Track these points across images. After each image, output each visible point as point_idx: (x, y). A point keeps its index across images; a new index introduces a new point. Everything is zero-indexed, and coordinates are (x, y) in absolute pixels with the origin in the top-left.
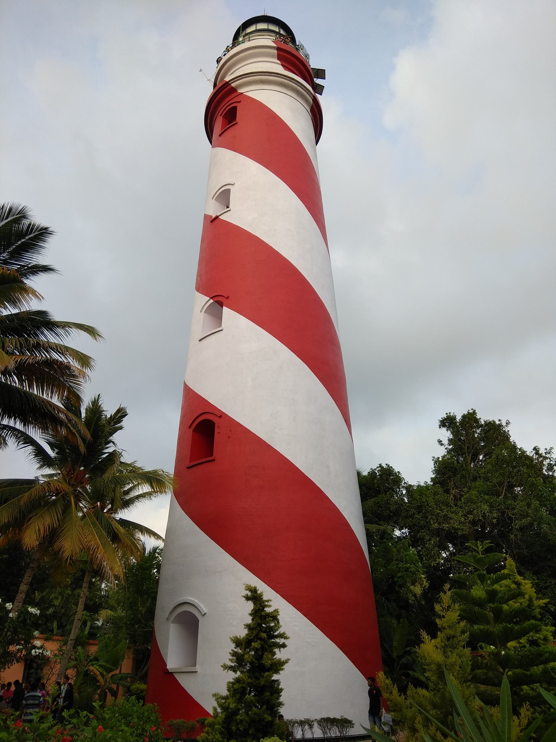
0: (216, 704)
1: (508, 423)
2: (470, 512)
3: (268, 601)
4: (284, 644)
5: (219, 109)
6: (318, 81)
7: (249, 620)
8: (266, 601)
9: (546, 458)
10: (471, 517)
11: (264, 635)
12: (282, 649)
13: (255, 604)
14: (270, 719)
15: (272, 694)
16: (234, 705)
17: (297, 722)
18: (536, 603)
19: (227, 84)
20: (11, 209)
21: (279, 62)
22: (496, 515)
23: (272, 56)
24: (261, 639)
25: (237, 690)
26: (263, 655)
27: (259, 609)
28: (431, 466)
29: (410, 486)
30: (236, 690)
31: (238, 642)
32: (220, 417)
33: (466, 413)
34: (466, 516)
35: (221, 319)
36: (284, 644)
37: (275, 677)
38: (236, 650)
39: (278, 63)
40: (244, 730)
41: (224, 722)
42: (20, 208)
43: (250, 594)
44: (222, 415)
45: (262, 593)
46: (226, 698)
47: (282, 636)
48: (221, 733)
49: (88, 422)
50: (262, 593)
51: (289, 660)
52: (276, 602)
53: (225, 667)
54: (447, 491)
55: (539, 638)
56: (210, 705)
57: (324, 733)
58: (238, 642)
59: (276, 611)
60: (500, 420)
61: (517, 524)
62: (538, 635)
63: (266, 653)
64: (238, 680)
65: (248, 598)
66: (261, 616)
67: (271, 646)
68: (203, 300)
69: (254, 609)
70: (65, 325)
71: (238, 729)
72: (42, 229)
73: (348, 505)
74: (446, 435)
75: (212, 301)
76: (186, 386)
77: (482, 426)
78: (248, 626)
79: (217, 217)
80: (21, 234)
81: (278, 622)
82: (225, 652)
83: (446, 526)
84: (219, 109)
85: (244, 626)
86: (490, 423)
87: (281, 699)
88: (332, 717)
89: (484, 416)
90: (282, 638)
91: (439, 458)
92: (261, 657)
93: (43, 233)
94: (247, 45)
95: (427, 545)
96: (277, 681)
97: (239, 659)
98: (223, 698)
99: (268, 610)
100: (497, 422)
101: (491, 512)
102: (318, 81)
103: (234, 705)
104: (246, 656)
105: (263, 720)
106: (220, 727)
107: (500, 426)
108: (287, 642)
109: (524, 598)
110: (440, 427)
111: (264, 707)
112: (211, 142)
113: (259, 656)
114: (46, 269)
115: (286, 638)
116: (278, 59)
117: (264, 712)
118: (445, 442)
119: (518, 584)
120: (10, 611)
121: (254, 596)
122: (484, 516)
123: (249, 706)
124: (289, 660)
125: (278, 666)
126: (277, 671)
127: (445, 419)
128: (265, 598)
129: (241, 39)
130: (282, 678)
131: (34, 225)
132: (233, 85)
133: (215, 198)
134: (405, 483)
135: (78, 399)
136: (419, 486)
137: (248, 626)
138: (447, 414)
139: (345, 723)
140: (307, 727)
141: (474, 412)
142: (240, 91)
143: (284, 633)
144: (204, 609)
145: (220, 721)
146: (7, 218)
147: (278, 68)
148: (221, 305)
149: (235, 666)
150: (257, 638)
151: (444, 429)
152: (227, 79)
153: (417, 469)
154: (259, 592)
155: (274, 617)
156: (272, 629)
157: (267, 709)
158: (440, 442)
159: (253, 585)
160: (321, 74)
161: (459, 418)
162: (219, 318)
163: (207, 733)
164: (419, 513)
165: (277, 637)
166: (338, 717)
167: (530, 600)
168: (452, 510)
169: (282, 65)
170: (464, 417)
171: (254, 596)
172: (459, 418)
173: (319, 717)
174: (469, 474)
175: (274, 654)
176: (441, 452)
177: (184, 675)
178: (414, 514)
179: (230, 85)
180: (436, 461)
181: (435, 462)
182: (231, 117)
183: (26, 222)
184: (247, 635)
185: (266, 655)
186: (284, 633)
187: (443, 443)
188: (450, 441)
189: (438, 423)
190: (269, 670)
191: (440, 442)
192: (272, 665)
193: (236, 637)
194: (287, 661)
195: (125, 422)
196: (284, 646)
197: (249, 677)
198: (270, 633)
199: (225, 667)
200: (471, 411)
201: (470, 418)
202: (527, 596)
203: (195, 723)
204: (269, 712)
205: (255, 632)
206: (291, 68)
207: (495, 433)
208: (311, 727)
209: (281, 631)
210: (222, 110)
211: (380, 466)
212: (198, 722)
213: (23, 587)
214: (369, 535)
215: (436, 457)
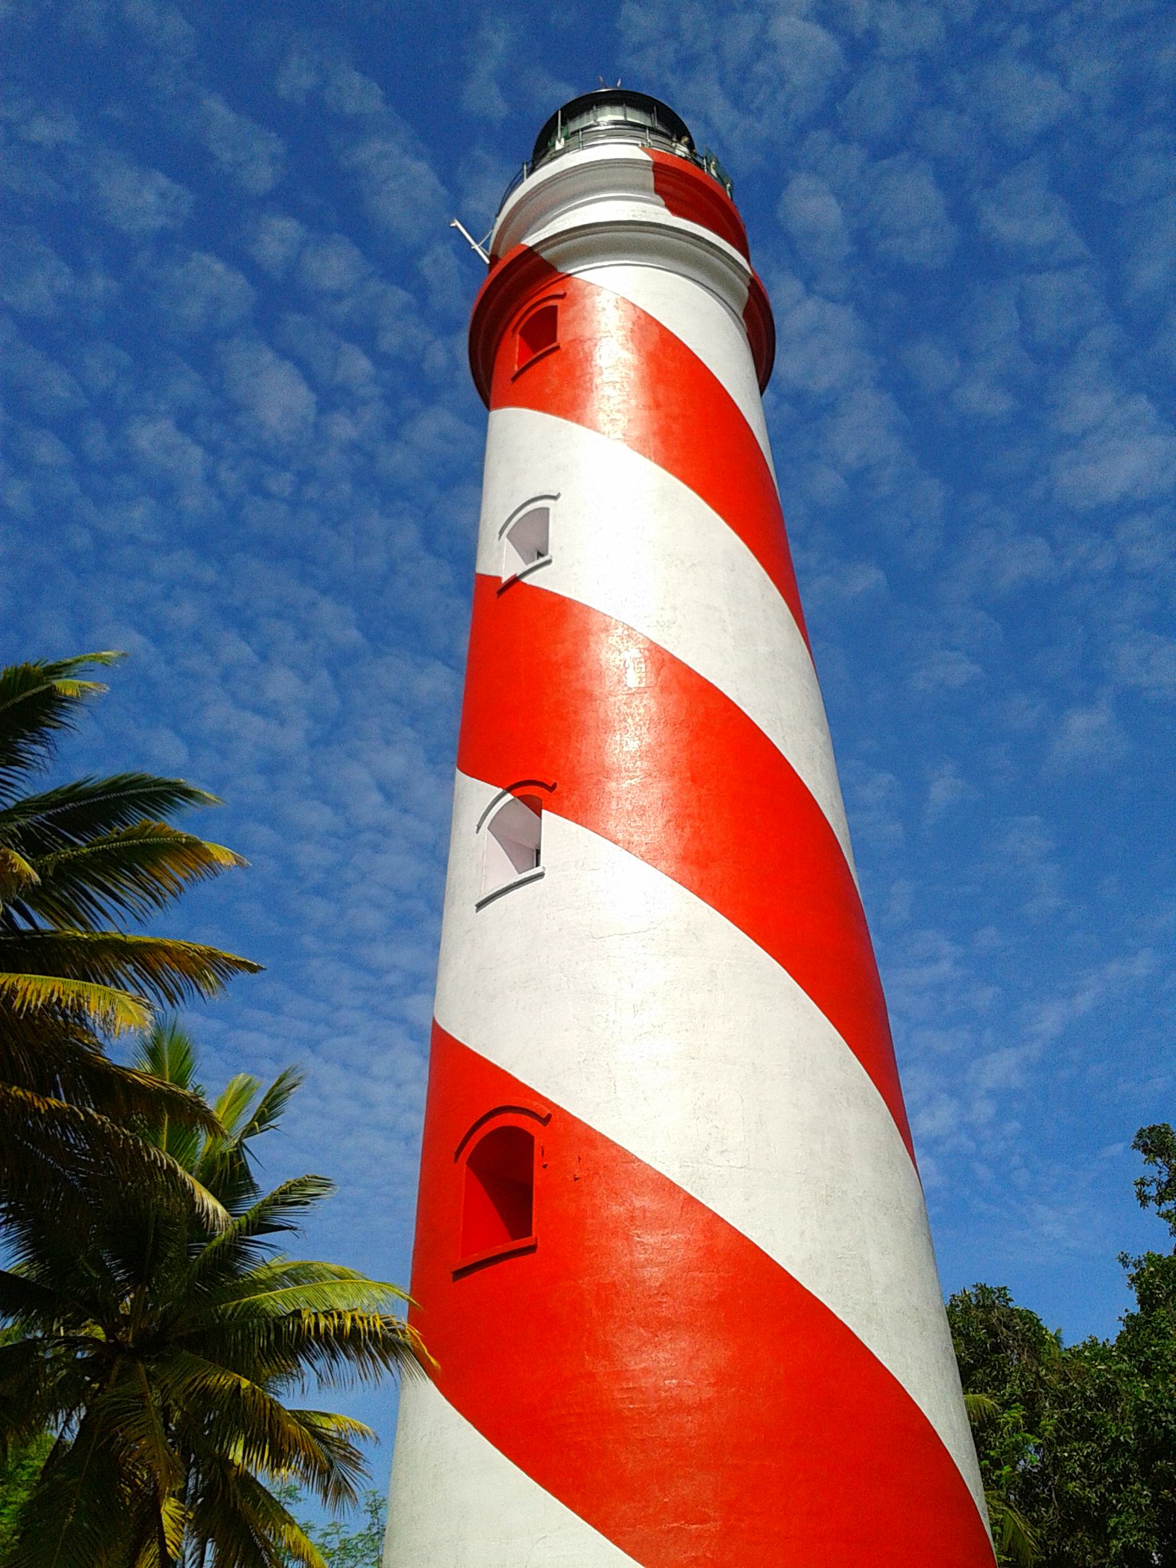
44: (550, 1116)
75: (509, 797)
79: (515, 580)
132: (544, 255)
148: (537, 809)
162: (529, 854)
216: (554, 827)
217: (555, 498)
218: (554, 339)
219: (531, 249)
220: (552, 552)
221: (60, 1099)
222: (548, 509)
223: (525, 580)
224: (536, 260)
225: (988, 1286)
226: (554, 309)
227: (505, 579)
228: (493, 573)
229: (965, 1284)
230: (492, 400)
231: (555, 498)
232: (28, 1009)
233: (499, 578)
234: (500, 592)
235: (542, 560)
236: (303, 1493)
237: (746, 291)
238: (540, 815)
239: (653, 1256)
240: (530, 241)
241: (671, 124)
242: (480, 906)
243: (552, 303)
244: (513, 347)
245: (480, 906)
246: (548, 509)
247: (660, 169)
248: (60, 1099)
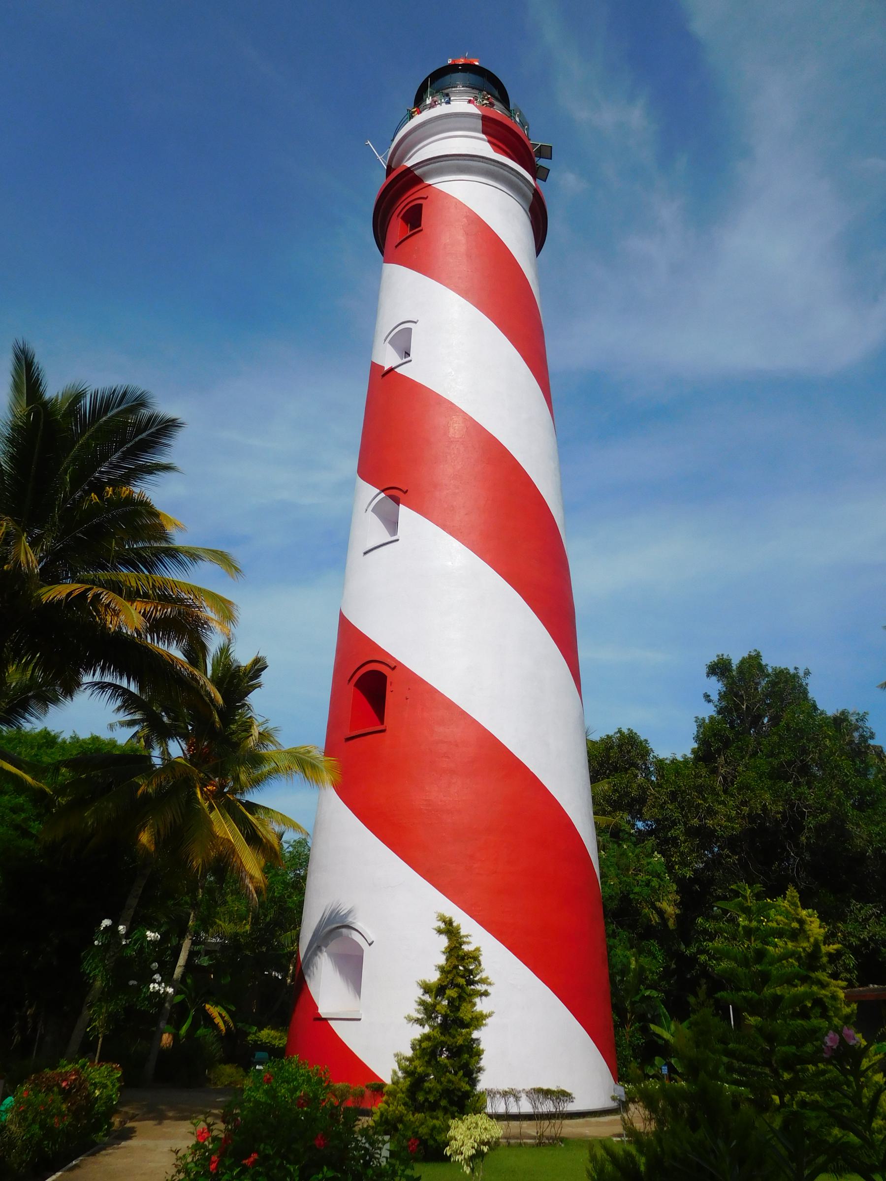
0: (396, 1068)
1: (807, 673)
2: (744, 803)
3: (467, 936)
4: (486, 991)
6: (541, 162)
7: (442, 960)
8: (464, 936)
9: (857, 729)
10: (746, 809)
11: (462, 981)
12: (483, 998)
13: (450, 939)
14: (468, 1088)
15: (471, 1057)
16: (422, 1068)
17: (499, 1093)
18: (824, 949)
19: (409, 170)
20: (125, 394)
21: (484, 136)
22: (781, 809)
24: (458, 986)
25: (426, 1050)
26: (460, 1005)
27: (455, 947)
28: (693, 729)
29: (661, 761)
30: (424, 1049)
31: (427, 989)
32: (395, 668)
33: (746, 655)
34: (739, 808)
35: (396, 523)
36: (486, 991)
37: (475, 1035)
38: (423, 998)
40: (435, 1101)
41: (408, 1090)
42: (138, 393)
43: (442, 926)
44: (396, 666)
45: (459, 925)
46: (411, 1060)
47: (483, 981)
48: (405, 1104)
49: (217, 682)
50: (459, 925)
51: (493, 1013)
52: (477, 937)
53: (409, 1019)
54: (714, 771)
55: (826, 996)
56: (386, 1069)
57: (535, 1107)
58: (427, 989)
59: (478, 949)
60: (796, 668)
61: (810, 822)
62: (823, 992)
63: (465, 1004)
64: (426, 1038)
65: (440, 931)
66: (458, 955)
67: (470, 995)
68: (369, 493)
69: (449, 947)
70: (194, 556)
71: (426, 1100)
72: (169, 421)
73: (570, 790)
74: (715, 686)
75: (383, 495)
76: (344, 622)
77: (768, 675)
78: (442, 969)
79: (391, 370)
80: (140, 428)
81: (480, 965)
82: (410, 1000)
83: (709, 822)
85: (434, 968)
86: (781, 671)
87: (482, 1063)
88: (545, 1087)
89: (772, 661)
90: (484, 984)
91: (704, 719)
92: (458, 1009)
93: (168, 426)
94: (442, 109)
95: (682, 849)
96: (477, 1039)
97: (429, 1010)
98: (407, 1059)
99: (466, 948)
100: (792, 671)
101: (774, 802)
102: (541, 162)
103: (422, 1068)
104: (438, 1008)
105: (459, 1090)
106: (403, 1096)
107: (795, 676)
108: (490, 989)
109: (809, 941)
110: (708, 676)
111: (461, 1073)
112: (382, 252)
113: (454, 1006)
114: (167, 468)
115: (490, 984)
116: (484, 132)
117: (460, 1080)
118: (715, 697)
119: (801, 922)
121: (450, 930)
122: (764, 808)
123: (442, 1070)
124: (493, 1013)
125: (478, 1021)
126: (477, 1027)
127: (716, 664)
128: (463, 932)
129: (428, 101)
130: (484, 1036)
131: (156, 417)
132: (417, 172)
134: (654, 756)
135: (204, 648)
136: (674, 761)
137: (442, 969)
138: (718, 656)
139: (563, 1095)
140: (512, 1099)
141: (758, 656)
143: (487, 978)
144: (371, 937)
145: (404, 1089)
146: (119, 405)
148: (397, 502)
149: (422, 1019)
150: (454, 984)
151: (714, 679)
153: (672, 739)
154: (455, 924)
155: (474, 957)
156: (471, 972)
157: (465, 1075)
158: (707, 698)
159: (448, 915)
160: (546, 152)
161: (735, 662)
162: (392, 524)
163: (387, 1103)
164: (672, 802)
165: (477, 982)
166: (553, 1088)
167: (816, 945)
168: (720, 799)
169: (489, 142)
170: (743, 661)
171: (450, 930)
172: (735, 662)
173: (528, 1088)
174: (747, 746)
175: (474, 1005)
176: (708, 711)
178: (665, 803)
180: (700, 723)
181: (699, 726)
183: (145, 412)
184: (439, 980)
185: (465, 1006)
186: (487, 978)
187: (711, 698)
188: (722, 696)
189: (705, 670)
190: (467, 1026)
191: (707, 698)
192: (472, 1019)
193: (425, 981)
194: (490, 1015)
195: (264, 677)
196: (486, 994)
197: (441, 1034)
198: (470, 978)
199: (409, 1019)
200: (753, 654)
201: (753, 663)
202: (812, 940)
203: (364, 1088)
204: (467, 1079)
205: (450, 976)
206: (505, 148)
207: (788, 688)
208: (517, 1099)
209: (483, 975)
211: (620, 731)
212: (367, 1087)
213: (133, 902)
214: (600, 830)
215: (700, 717)
216: (404, 511)
218: (420, 225)
219: (409, 168)
221: (39, 563)
224: (410, 175)
225: (434, 977)
226: (420, 206)
229: (605, 728)
234: (383, 376)
235: (407, 359)
239: (456, 429)
240: (409, 164)
242: (365, 553)
244: (396, 227)
245: (365, 553)
247: (485, 119)
248: (39, 563)
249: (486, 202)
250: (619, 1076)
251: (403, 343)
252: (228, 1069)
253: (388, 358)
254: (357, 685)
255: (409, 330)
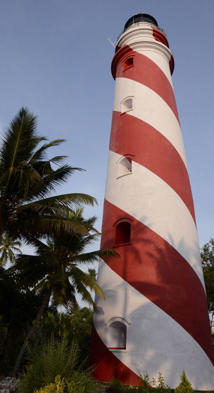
5: (122, 58)
19: (128, 46)
21: (153, 37)
23: (150, 34)
35: (157, 25)
39: (153, 38)
68: (119, 157)
75: (124, 157)
79: (125, 113)
80: (90, 363)
84: (122, 58)
120: (56, 304)
132: (131, 47)
133: (129, 243)
142: (134, 50)
147: (153, 39)
152: (128, 44)
158: (5, 392)
162: (130, 169)
177: (129, 112)
179: (129, 47)
182: (130, 62)
191: (5, 392)
206: (158, 40)
210: (125, 58)
217: (134, 56)
219: (128, 46)
220: (133, 108)
222: (132, 99)
223: (127, 113)
227: (122, 113)
228: (119, 111)
230: (117, 74)
231: (134, 56)
232: (14, 123)
233: (121, 113)
234: (121, 115)
236: (77, 263)
237: (170, 57)
238: (131, 163)
241: (153, 21)
243: (132, 57)
244: (121, 67)
246: (132, 99)
249: (157, 57)
250: (171, 389)
251: (129, 103)
252: (9, 391)
253: (123, 109)
254: (117, 227)
255: (131, 100)
